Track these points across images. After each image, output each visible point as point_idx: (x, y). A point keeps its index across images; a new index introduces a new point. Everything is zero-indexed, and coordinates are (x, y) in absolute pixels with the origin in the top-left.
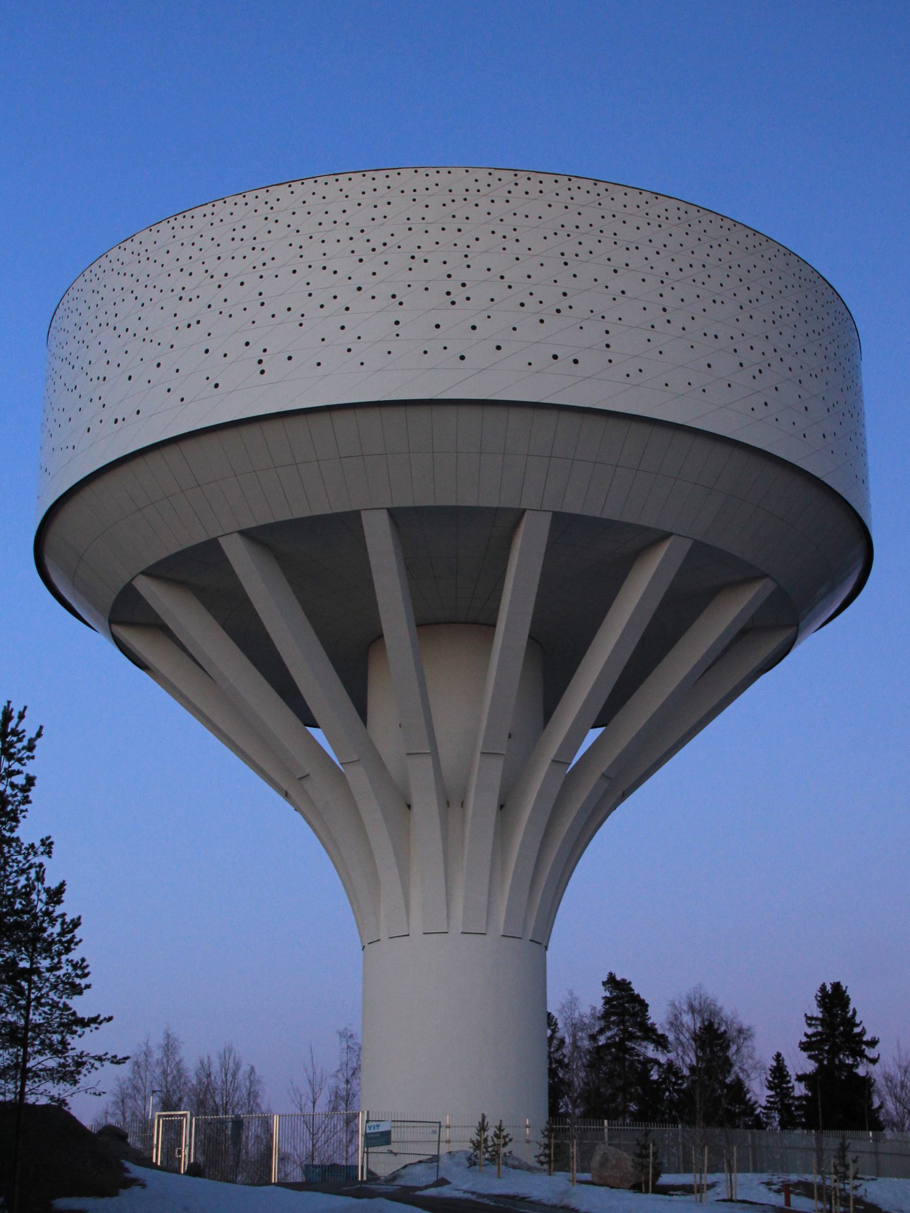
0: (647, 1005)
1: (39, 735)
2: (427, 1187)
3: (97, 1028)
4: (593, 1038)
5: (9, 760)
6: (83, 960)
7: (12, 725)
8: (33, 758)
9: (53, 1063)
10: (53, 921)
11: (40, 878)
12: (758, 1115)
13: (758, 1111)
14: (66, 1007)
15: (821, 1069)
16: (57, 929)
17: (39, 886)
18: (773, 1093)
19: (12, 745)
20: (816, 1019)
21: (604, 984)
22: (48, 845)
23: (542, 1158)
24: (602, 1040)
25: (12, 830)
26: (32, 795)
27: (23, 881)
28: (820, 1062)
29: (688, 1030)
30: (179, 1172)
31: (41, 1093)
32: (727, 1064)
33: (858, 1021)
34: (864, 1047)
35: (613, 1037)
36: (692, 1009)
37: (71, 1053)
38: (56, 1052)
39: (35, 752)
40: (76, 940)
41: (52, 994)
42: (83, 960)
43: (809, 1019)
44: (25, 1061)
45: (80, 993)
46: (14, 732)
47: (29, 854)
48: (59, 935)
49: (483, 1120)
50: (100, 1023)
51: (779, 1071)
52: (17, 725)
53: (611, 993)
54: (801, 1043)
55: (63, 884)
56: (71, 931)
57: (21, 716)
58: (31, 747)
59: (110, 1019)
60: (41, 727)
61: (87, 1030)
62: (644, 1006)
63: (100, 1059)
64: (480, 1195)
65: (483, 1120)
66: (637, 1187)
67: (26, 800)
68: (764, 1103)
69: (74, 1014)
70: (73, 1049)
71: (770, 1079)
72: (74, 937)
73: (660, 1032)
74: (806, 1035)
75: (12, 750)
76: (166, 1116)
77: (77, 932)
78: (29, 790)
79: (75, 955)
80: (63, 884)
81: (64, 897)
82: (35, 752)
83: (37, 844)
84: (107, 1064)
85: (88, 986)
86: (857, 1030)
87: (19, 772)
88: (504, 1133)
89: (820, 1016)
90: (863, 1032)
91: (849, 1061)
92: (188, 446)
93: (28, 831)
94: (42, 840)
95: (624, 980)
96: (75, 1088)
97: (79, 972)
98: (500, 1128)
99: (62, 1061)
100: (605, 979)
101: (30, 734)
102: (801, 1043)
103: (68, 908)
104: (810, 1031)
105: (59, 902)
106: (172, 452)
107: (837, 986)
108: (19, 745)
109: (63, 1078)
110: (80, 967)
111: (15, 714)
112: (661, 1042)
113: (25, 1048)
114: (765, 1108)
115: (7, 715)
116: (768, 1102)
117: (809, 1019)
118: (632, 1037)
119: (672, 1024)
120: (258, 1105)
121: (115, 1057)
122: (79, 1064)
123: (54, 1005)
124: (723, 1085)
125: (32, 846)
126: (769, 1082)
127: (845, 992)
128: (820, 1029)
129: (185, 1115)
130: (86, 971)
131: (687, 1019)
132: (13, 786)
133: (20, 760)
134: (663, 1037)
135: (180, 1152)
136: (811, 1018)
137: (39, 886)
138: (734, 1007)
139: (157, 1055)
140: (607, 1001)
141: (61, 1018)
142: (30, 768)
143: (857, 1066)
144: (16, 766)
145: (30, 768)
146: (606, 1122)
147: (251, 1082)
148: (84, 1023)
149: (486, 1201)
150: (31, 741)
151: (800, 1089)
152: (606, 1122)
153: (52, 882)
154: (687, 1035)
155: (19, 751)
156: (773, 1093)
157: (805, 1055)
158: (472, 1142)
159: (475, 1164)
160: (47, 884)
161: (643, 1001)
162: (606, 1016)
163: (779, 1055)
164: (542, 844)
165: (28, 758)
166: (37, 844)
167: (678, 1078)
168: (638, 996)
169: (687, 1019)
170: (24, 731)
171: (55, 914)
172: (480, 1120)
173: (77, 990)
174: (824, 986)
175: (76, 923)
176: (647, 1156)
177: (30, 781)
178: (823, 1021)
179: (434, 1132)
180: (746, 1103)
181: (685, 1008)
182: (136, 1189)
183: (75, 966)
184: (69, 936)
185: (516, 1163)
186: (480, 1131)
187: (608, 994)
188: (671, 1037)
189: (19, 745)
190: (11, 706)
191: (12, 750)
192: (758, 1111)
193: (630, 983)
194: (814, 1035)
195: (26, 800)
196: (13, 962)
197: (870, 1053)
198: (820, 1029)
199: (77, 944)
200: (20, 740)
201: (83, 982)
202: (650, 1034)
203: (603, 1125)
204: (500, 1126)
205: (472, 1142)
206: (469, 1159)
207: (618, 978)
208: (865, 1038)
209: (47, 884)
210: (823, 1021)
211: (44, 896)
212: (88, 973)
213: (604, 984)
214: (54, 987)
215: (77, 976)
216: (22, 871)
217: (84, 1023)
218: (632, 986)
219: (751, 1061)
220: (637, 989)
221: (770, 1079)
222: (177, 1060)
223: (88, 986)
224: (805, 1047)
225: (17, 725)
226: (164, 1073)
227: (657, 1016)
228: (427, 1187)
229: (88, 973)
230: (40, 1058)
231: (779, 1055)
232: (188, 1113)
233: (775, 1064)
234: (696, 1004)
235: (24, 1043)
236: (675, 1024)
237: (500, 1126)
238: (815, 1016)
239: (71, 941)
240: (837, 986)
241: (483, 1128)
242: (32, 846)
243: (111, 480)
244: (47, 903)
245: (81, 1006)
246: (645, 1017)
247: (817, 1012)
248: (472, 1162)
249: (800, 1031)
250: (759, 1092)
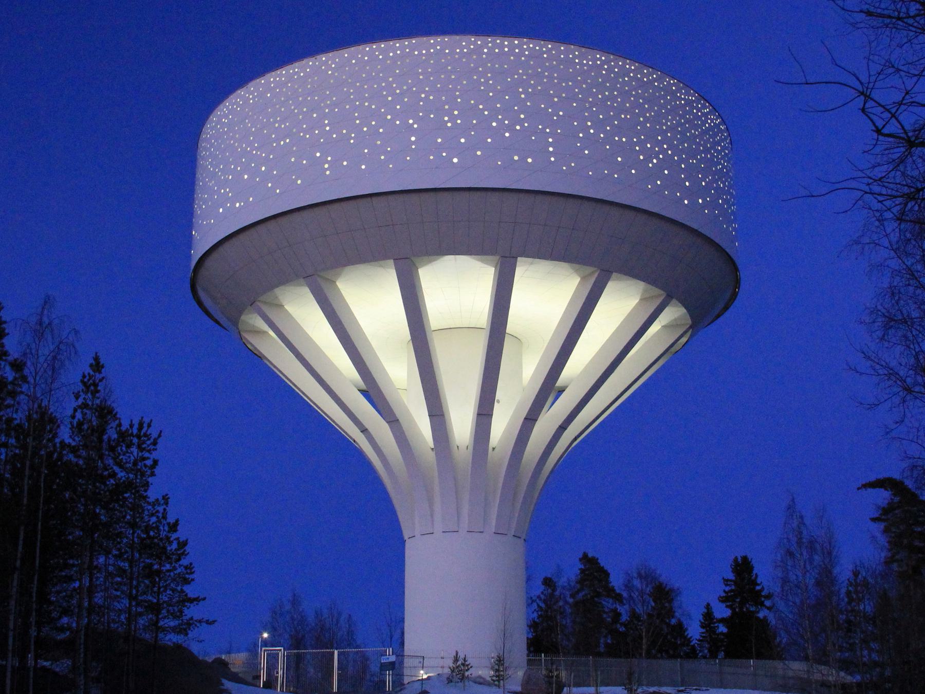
1: (160, 436)
10: (171, 543)
11: (164, 517)
14: (182, 591)
15: (734, 613)
16: (175, 546)
17: (164, 522)
18: (704, 630)
19: (144, 442)
20: (731, 581)
22: (166, 499)
24: (580, 596)
28: (733, 609)
29: (637, 590)
32: (671, 613)
35: (586, 595)
36: (640, 576)
37: (184, 618)
38: (175, 617)
42: (191, 564)
43: (726, 581)
44: (157, 622)
46: (145, 435)
51: (708, 615)
55: (177, 521)
57: (149, 426)
58: (155, 443)
61: (192, 605)
62: (607, 574)
63: (200, 621)
67: (153, 474)
68: (698, 637)
69: (186, 595)
73: (618, 591)
74: (724, 591)
77: (186, 548)
79: (185, 562)
80: (177, 521)
81: (179, 528)
82: (158, 446)
84: (204, 624)
85: (193, 580)
86: (758, 588)
87: (148, 458)
90: (763, 589)
92: (283, 221)
93: (153, 494)
98: (465, 660)
103: (181, 533)
104: (727, 589)
105: (176, 531)
106: (272, 225)
107: (745, 559)
108: (149, 442)
109: (180, 632)
111: (145, 425)
112: (618, 598)
114: (699, 640)
117: (726, 581)
119: (626, 586)
120: (354, 640)
123: (173, 590)
124: (668, 625)
125: (157, 500)
128: (733, 587)
131: (637, 583)
133: (149, 451)
134: (620, 595)
136: (727, 580)
137: (164, 522)
138: (670, 573)
142: (154, 455)
143: (758, 612)
144: (147, 455)
145: (154, 455)
147: (350, 625)
148: (191, 601)
151: (722, 629)
153: (171, 519)
160: (168, 521)
161: (606, 571)
162: (581, 582)
163: (708, 605)
164: (457, 498)
167: (639, 621)
169: (637, 583)
173: (187, 582)
174: (736, 557)
175: (185, 543)
176: (552, 677)
177: (156, 462)
178: (735, 583)
180: (686, 637)
181: (635, 575)
183: (186, 568)
188: (625, 594)
189: (149, 442)
194: (731, 591)
195: (153, 474)
197: (768, 603)
198: (733, 587)
200: (149, 439)
201: (191, 577)
202: (610, 592)
207: (590, 555)
209: (168, 521)
211: (166, 528)
214: (174, 580)
215: (187, 573)
216: (153, 515)
217: (191, 601)
219: (680, 611)
220: (602, 563)
223: (193, 580)
224: (723, 600)
226: (292, 619)
227: (616, 581)
231: (708, 605)
236: (628, 586)
239: (183, 554)
240: (745, 559)
241: (456, 659)
245: (191, 591)
246: (608, 582)
247: (731, 576)
249: (721, 590)
250: (694, 631)
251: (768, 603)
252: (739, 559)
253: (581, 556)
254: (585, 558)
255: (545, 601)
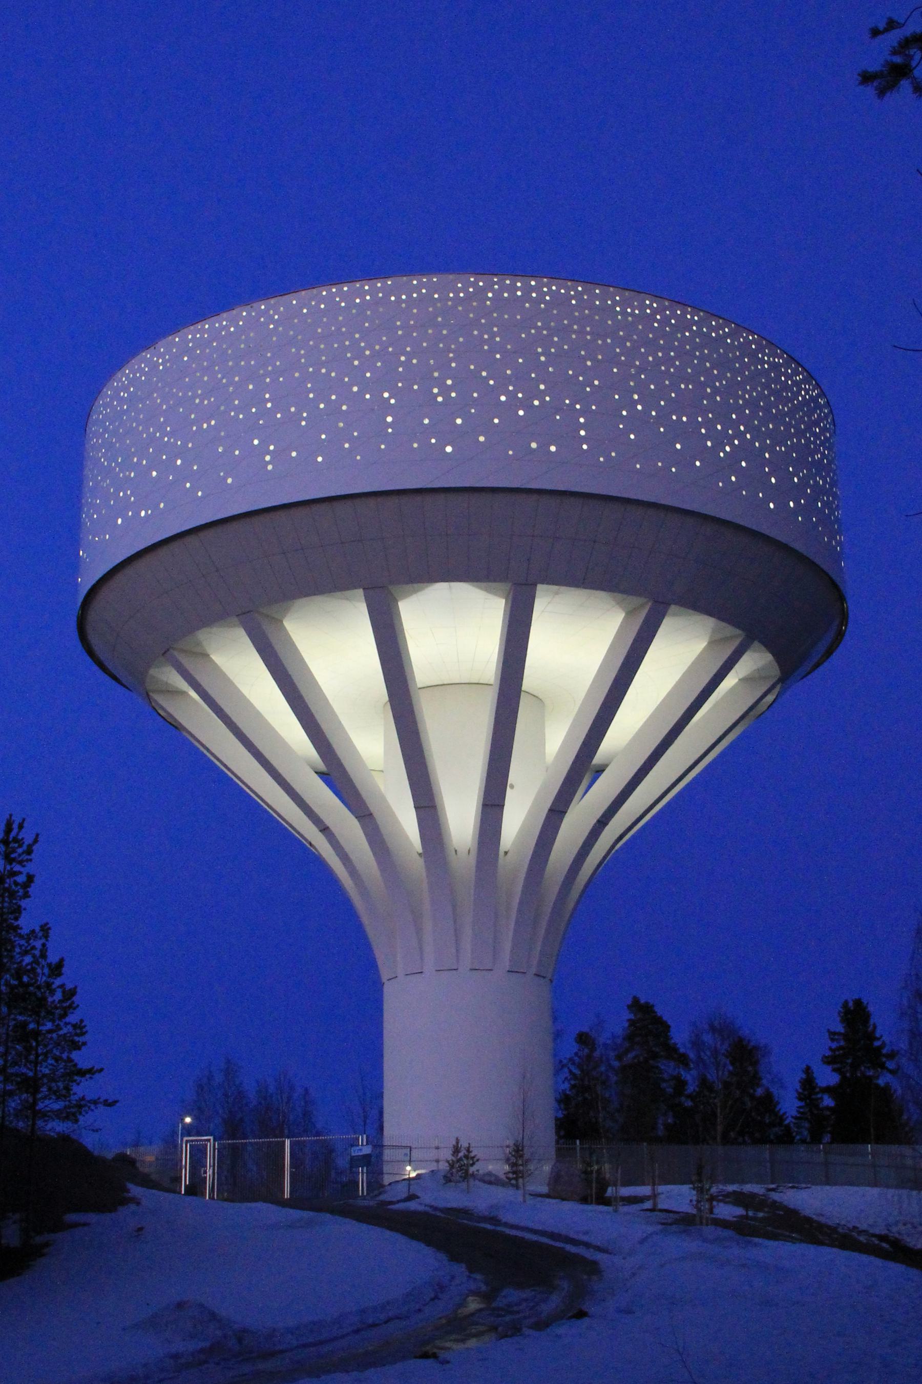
0: (670, 1027)
1: (36, 841)
2: (399, 1202)
3: (91, 1078)
4: (619, 1058)
5: (11, 864)
6: (82, 1021)
7: (13, 834)
8: (31, 860)
9: (56, 1106)
11: (44, 955)
12: (789, 1124)
13: (787, 1122)
14: (70, 1060)
17: (43, 962)
18: (803, 1104)
19: (14, 851)
20: (839, 1034)
21: (629, 1007)
22: (45, 929)
23: (511, 1175)
25: (16, 919)
26: (31, 890)
27: (28, 959)
30: (177, 1192)
31: (57, 1127)
33: (878, 1035)
34: (884, 1059)
39: (33, 856)
40: (75, 1005)
41: (55, 1051)
43: (832, 1035)
45: (79, 1048)
46: (16, 840)
47: (30, 939)
48: (60, 1001)
49: (457, 1143)
50: (93, 1074)
52: (18, 834)
53: (635, 1015)
54: (824, 1056)
56: (70, 999)
57: (21, 826)
58: (29, 852)
59: (101, 1070)
60: (37, 835)
64: (436, 1209)
65: (457, 1143)
66: (585, 1200)
68: (794, 1113)
69: (76, 1065)
70: (75, 1094)
71: (800, 1091)
72: (73, 1002)
73: (682, 1050)
74: (830, 1049)
75: (13, 856)
76: (192, 1141)
78: (29, 886)
79: (73, 1018)
81: (64, 970)
83: (37, 929)
85: (84, 1044)
86: (877, 1043)
88: (472, 1155)
89: (843, 1031)
91: (871, 1073)
93: (26, 923)
94: (41, 927)
95: (647, 1003)
96: (76, 1126)
97: (78, 1031)
98: (468, 1150)
99: (67, 1103)
100: (630, 1003)
101: (27, 842)
102: (824, 1056)
103: (67, 979)
104: (834, 1045)
107: (858, 1003)
108: (20, 850)
109: (67, 1118)
110: (79, 1028)
112: (683, 1060)
113: (34, 1095)
114: (796, 1118)
115: (9, 829)
116: (799, 1112)
117: (832, 1035)
118: (655, 1056)
121: (106, 1101)
122: (80, 1107)
125: (33, 931)
126: (799, 1094)
127: (866, 1007)
128: (842, 1043)
129: (209, 1140)
130: (84, 1030)
131: (707, 1038)
132: (16, 883)
133: (20, 863)
135: (205, 1172)
136: (834, 1033)
137: (43, 962)
139: (219, 1078)
140: (632, 1023)
141: (65, 1069)
143: (878, 1078)
144: (17, 868)
145: (30, 868)
146: (578, 1142)
147: (306, 1102)
148: (82, 1073)
149: (438, 1214)
150: (30, 846)
151: (828, 1101)
152: (578, 1142)
153: (53, 958)
154: (708, 1053)
155: (20, 855)
156: (803, 1104)
157: (830, 1068)
158: (448, 1162)
159: (450, 1181)
161: (666, 1022)
162: (630, 1038)
165: (27, 860)
166: (37, 929)
168: (660, 1018)
169: (707, 1038)
170: (23, 839)
171: (54, 986)
172: (454, 1143)
173: (77, 1046)
174: (846, 1002)
175: (73, 992)
177: (30, 878)
178: (845, 1036)
179: (406, 1155)
181: (706, 1027)
182: (133, 1207)
183: (75, 1026)
184: (70, 1002)
185: (493, 1179)
186: (454, 1152)
187: (632, 1016)
188: (692, 1055)
189: (20, 850)
190: (13, 818)
191: (13, 856)
192: (787, 1122)
193: (653, 1006)
195: (26, 895)
196: (24, 1025)
197: (891, 1065)
199: (75, 1009)
200: (20, 846)
202: (671, 1051)
203: (576, 1144)
204: (469, 1147)
205: (448, 1162)
206: (445, 1177)
208: (884, 1051)
210: (845, 1036)
211: (46, 971)
212: (87, 1032)
213: (629, 1007)
214: (57, 1044)
215: (77, 1035)
216: (26, 953)
217: (82, 1073)
218: (656, 1009)
220: (659, 1010)
221: (800, 1091)
222: (237, 1083)
223: (84, 1044)
225: (18, 834)
227: (680, 1037)
228: (399, 1202)
229: (87, 1032)
230: (47, 1102)
232: (211, 1138)
233: (804, 1076)
234: (716, 1023)
235: (36, 1090)
236: (697, 1044)
237: (469, 1147)
238: (837, 1030)
239: (70, 1007)
240: (858, 1003)
241: (456, 1150)
242: (33, 931)
243: (141, 565)
244: (49, 976)
245: (82, 1059)
247: (840, 1028)
248: (448, 1179)
249: (824, 1046)
250: (789, 1105)
251: (891, 1065)
252: (851, 1004)
253: (629, 1001)
254: (636, 1005)
255: (579, 1066)
